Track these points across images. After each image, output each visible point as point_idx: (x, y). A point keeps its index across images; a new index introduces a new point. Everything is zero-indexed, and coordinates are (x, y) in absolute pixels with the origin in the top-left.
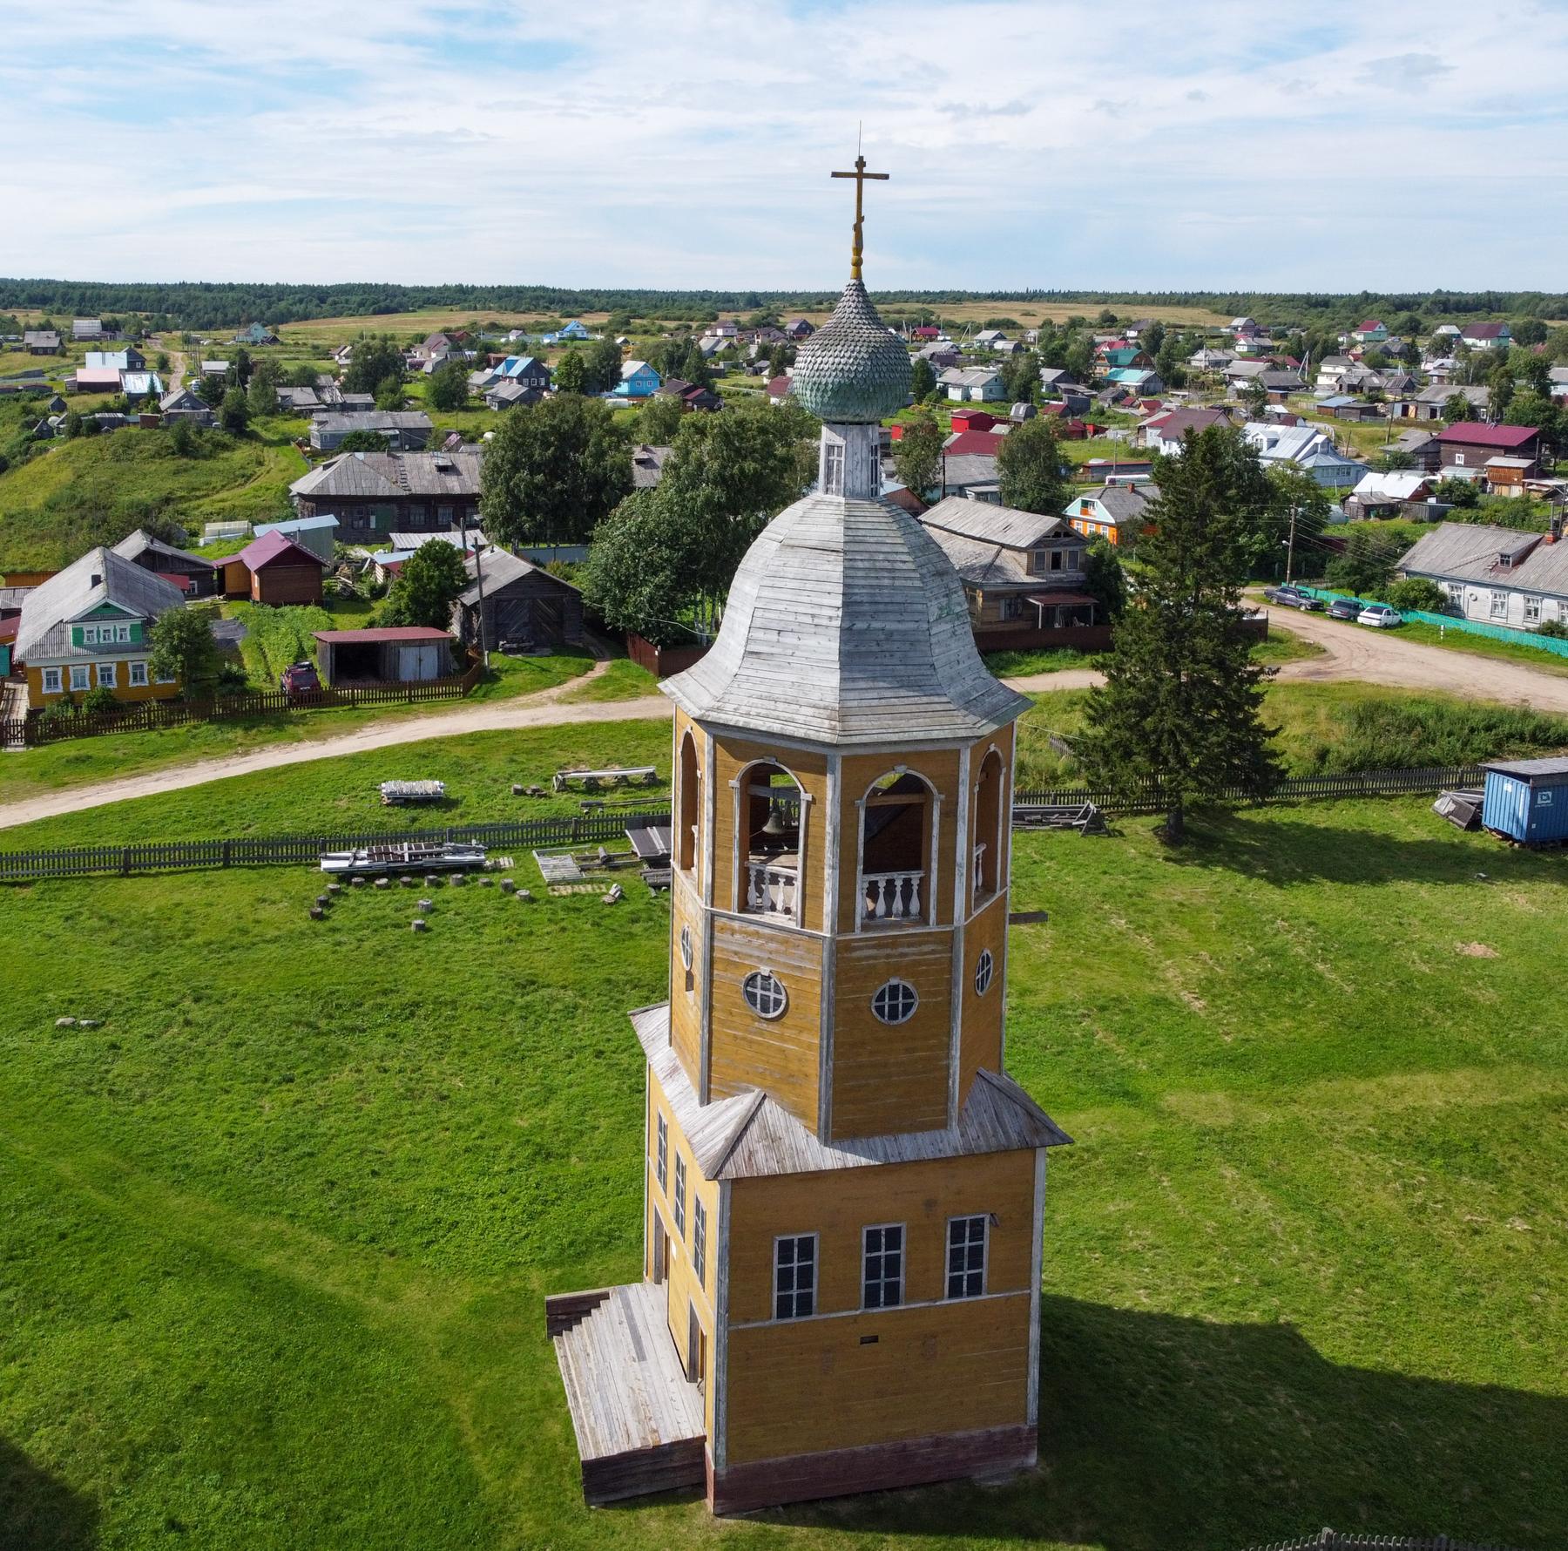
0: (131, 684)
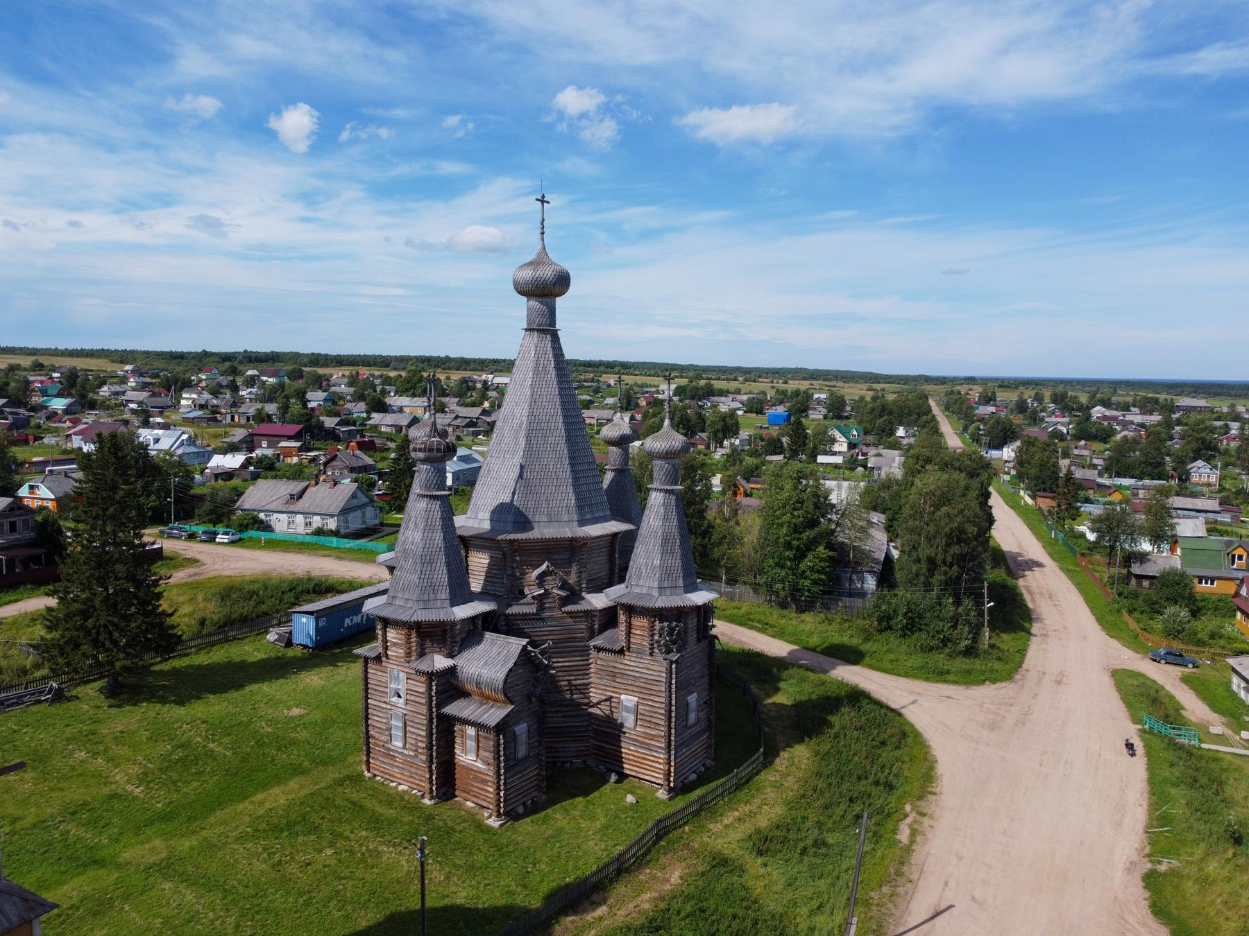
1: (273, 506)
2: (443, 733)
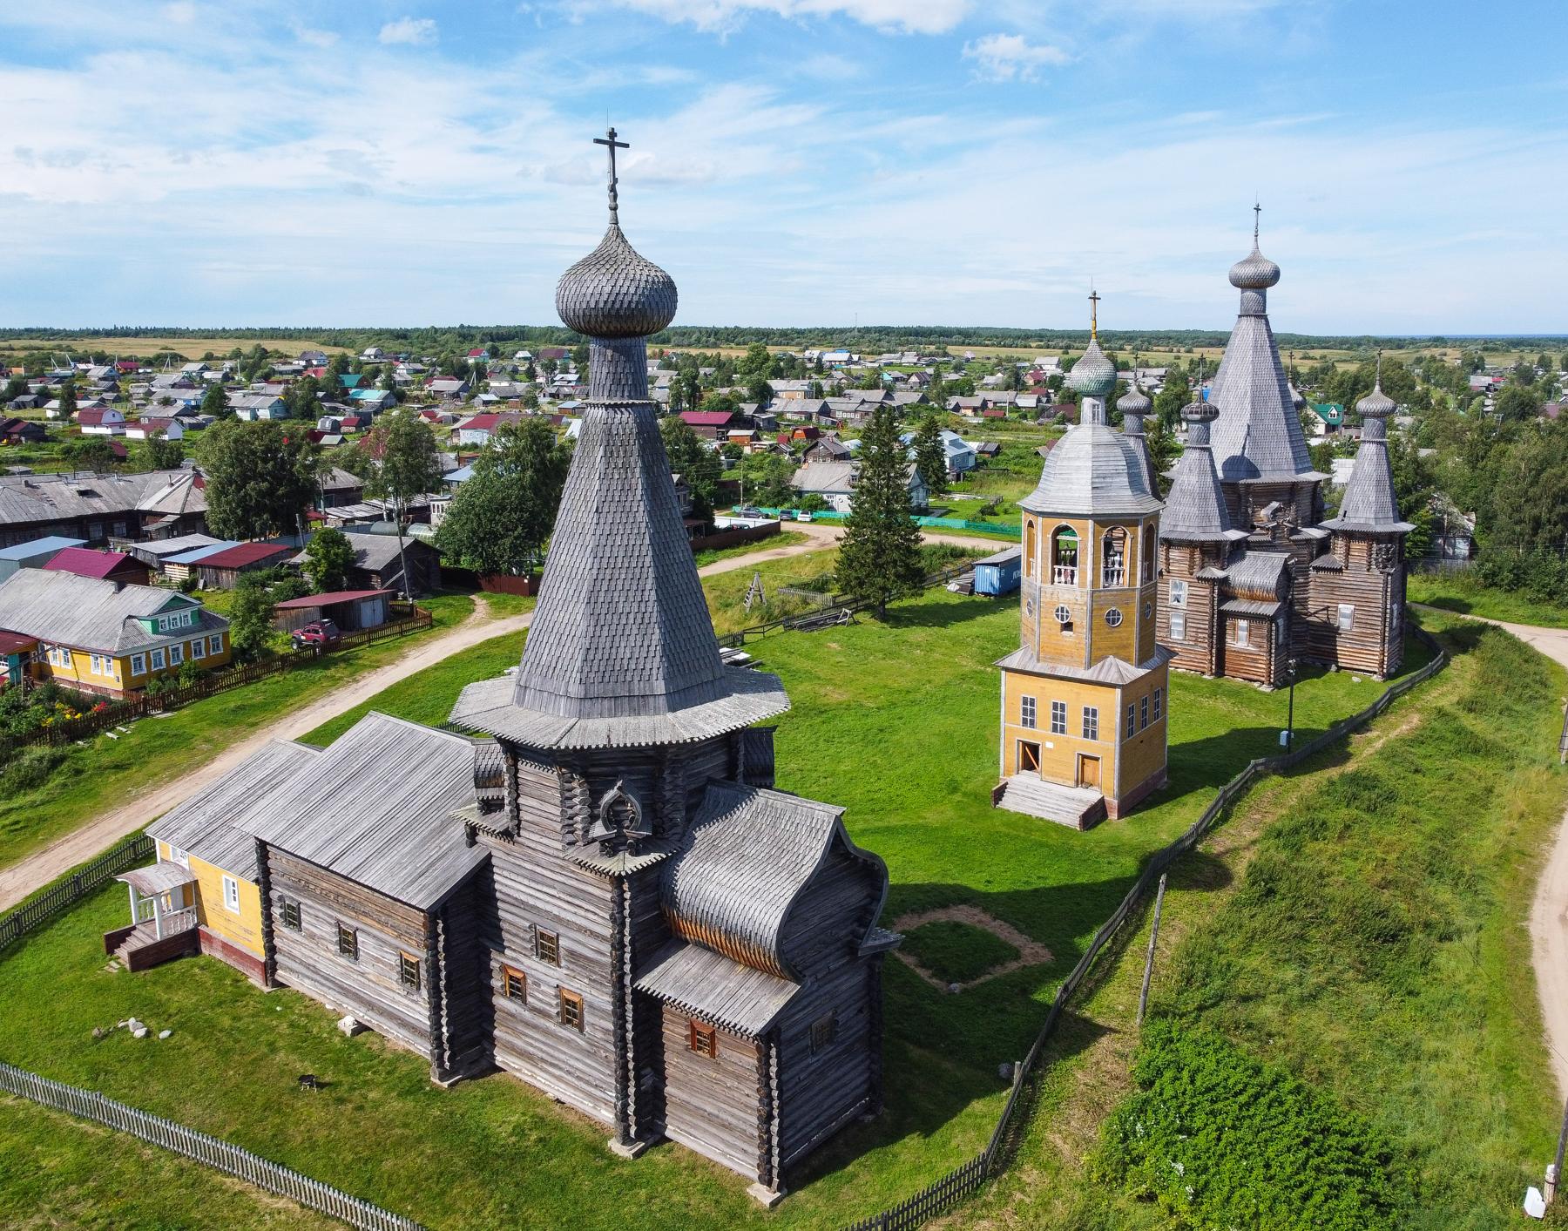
0: (134, 674)
1: (836, 487)
2: (1220, 624)
